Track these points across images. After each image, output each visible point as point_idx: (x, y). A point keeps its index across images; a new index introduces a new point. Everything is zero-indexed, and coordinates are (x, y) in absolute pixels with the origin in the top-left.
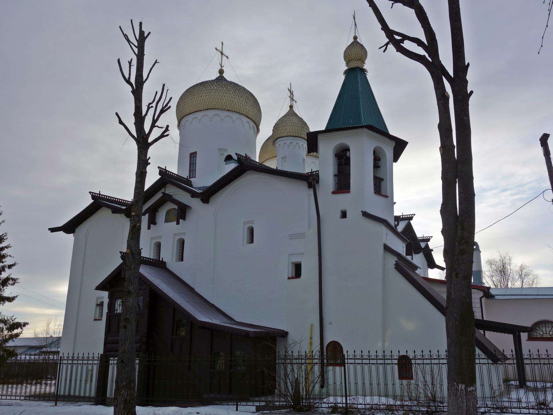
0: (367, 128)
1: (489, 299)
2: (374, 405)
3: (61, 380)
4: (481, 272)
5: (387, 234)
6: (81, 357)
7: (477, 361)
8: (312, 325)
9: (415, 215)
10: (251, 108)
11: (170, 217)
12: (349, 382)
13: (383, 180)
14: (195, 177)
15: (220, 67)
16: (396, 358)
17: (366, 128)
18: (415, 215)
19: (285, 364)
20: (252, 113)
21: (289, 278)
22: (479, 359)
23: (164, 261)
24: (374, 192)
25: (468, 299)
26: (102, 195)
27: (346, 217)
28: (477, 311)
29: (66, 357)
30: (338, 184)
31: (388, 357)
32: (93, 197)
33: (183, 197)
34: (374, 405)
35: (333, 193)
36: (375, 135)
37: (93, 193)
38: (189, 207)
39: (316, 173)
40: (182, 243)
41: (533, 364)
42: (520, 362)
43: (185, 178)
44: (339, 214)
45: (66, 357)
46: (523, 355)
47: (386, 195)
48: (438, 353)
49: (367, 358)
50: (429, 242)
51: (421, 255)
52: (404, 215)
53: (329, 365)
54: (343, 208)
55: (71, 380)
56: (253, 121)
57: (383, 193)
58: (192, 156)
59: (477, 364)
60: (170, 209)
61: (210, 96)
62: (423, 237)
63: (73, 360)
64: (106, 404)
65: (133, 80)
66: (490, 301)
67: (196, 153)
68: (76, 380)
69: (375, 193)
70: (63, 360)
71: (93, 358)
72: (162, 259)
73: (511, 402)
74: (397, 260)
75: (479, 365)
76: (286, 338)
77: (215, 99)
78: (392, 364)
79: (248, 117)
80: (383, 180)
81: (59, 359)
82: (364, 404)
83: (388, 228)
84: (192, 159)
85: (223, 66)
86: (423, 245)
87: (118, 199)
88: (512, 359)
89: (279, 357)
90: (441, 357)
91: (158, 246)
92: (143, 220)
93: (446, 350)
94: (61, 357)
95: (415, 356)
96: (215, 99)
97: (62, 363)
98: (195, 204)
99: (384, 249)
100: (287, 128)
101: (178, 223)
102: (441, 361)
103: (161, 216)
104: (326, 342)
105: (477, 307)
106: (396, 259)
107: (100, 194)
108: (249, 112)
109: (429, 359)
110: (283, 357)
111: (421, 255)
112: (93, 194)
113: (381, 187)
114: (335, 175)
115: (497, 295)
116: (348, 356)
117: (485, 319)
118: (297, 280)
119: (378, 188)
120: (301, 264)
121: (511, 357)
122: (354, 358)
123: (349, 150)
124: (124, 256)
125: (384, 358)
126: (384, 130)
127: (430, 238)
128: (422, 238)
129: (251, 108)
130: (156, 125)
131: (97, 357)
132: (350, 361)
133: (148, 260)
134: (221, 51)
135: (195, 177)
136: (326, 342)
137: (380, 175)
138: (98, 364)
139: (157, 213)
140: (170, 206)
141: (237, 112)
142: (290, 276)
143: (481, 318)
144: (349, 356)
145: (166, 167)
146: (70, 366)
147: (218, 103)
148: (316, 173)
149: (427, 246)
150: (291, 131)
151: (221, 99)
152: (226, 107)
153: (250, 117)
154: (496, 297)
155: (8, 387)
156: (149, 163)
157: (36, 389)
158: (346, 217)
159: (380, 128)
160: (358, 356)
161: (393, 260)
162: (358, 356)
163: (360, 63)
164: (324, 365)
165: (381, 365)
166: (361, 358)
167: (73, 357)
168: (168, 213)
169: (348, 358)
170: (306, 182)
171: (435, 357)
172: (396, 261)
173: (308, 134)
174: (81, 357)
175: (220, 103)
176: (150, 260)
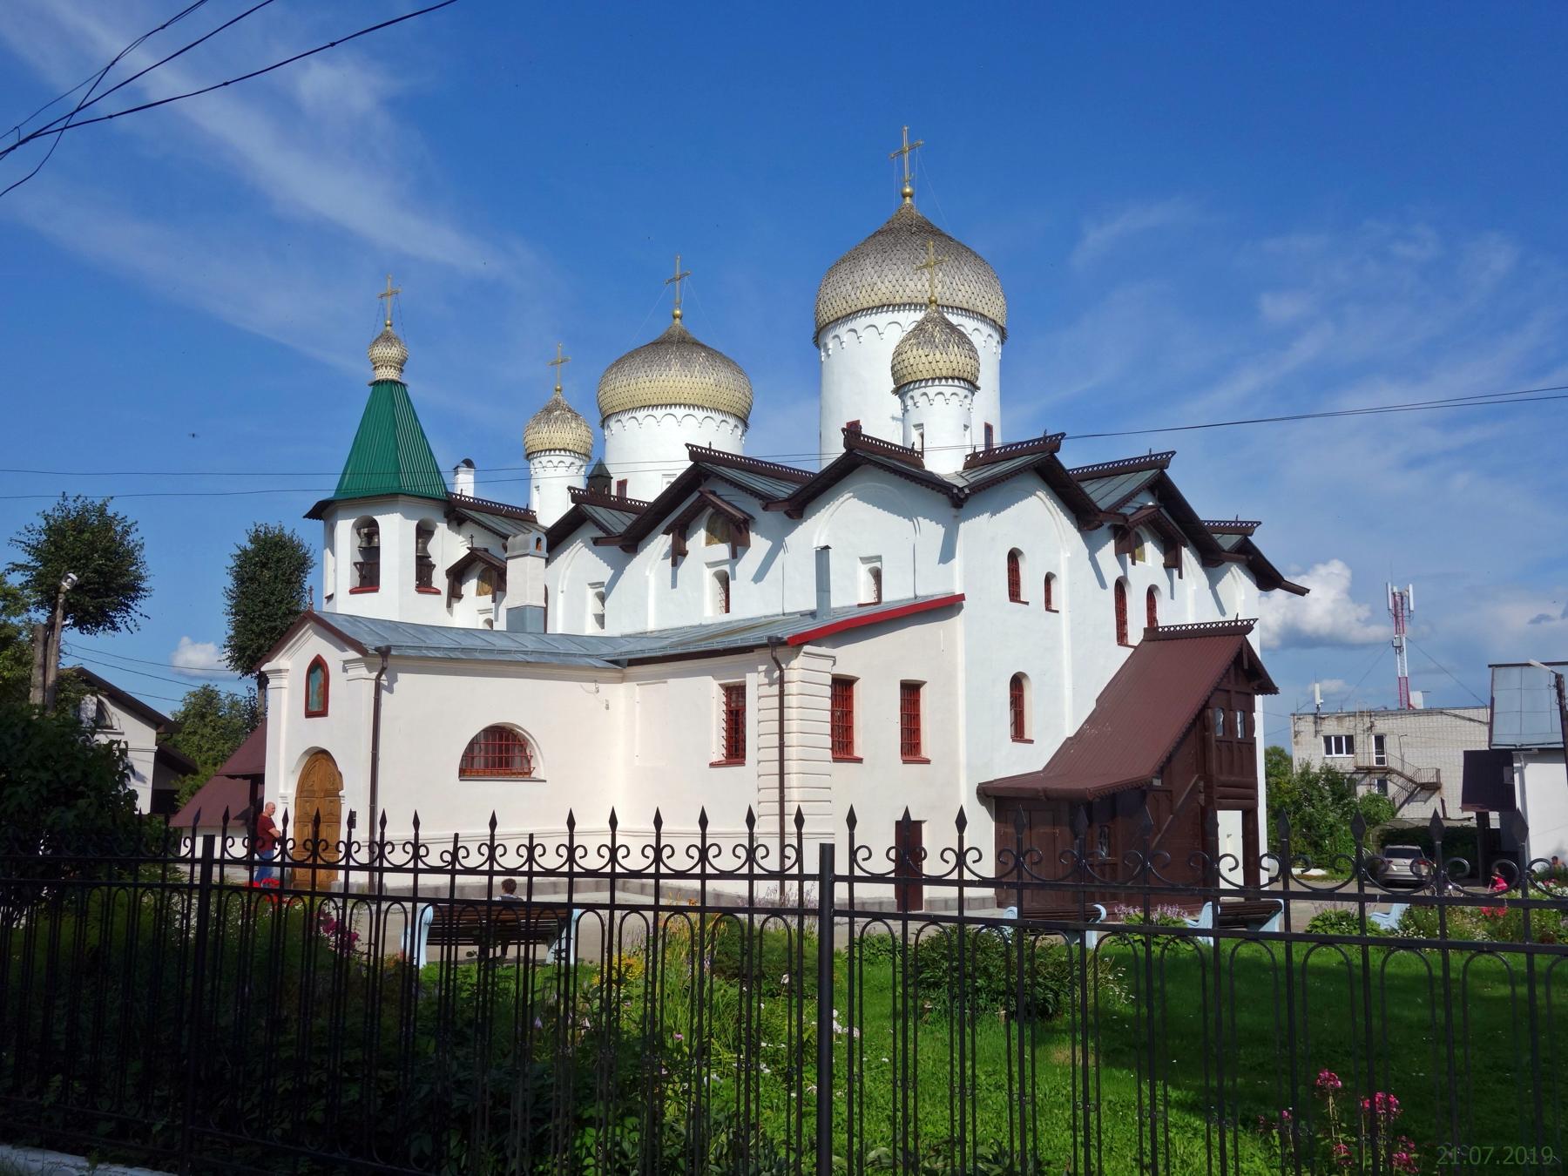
6: (680, 848)
9: (1174, 453)
18: (1174, 453)
21: (712, 765)
26: (715, 451)
29: (727, 849)
37: (693, 446)
39: (1145, 460)
42: (422, 1095)
45: (727, 849)
46: (893, 854)
50: (1167, 468)
52: (1154, 455)
70: (851, 879)
76: (1268, 747)
81: (812, 865)
87: (699, 447)
94: (827, 852)
107: (710, 449)
110: (363, 857)
116: (853, 853)
122: (955, 876)
124: (576, 496)
148: (1145, 460)
166: (310, 861)
169: (858, 872)
174: (680, 848)
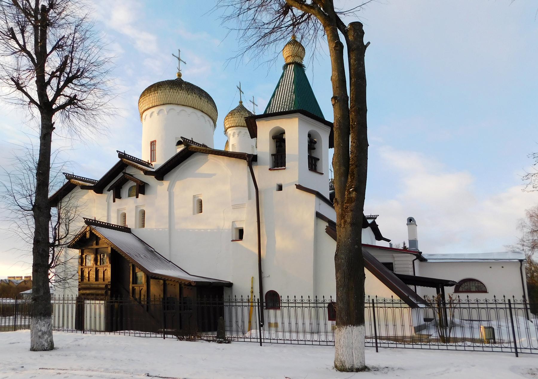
0: (301, 113)
1: (422, 262)
4: (416, 242)
5: (320, 204)
8: (253, 277)
10: (205, 104)
11: (132, 192)
13: (318, 159)
14: (156, 161)
15: (178, 70)
17: (299, 112)
20: (207, 108)
22: (377, 303)
23: (128, 227)
24: (309, 169)
25: (356, 246)
27: (282, 190)
28: (410, 270)
30: (274, 162)
31: (239, 301)
32: (67, 177)
33: (141, 176)
35: (270, 169)
36: (314, 122)
38: (147, 184)
40: (143, 213)
41: (453, 308)
43: (146, 162)
44: (275, 187)
45: (75, 298)
47: (321, 172)
51: (369, 229)
53: (268, 308)
55: (63, 316)
56: (208, 115)
57: (318, 171)
58: (153, 144)
60: (133, 186)
61: (165, 93)
62: (371, 216)
63: (64, 300)
65: (30, 47)
66: (423, 263)
67: (155, 141)
69: (309, 170)
71: (72, 299)
72: (127, 226)
73: (488, 320)
74: (328, 225)
77: (170, 96)
79: (203, 112)
80: (318, 159)
83: (321, 199)
84: (152, 146)
85: (180, 70)
86: (370, 221)
91: (124, 216)
95: (324, 301)
96: (170, 96)
98: (151, 180)
99: (316, 216)
100: (236, 119)
101: (137, 197)
103: (125, 191)
104: (266, 290)
105: (410, 267)
106: (327, 224)
108: (204, 107)
111: (369, 229)
112: (66, 175)
113: (316, 166)
114: (272, 155)
115: (429, 259)
117: (416, 275)
118: (240, 242)
119: (314, 167)
120: (243, 229)
123: (284, 133)
125: (316, 302)
126: (319, 116)
127: (377, 216)
128: (370, 216)
129: (205, 104)
130: (61, 93)
132: (379, 305)
133: (120, 227)
134: (178, 57)
135: (156, 161)
136: (266, 290)
137: (314, 155)
138: (281, 303)
139: (121, 190)
140: (132, 184)
141: (189, 106)
142: (234, 239)
143: (411, 274)
145: (124, 151)
146: (61, 306)
147: (173, 99)
149: (374, 222)
150: (239, 122)
151: (175, 96)
152: (181, 102)
154: (429, 261)
155: (9, 319)
156: (54, 128)
157: (21, 322)
158: (282, 190)
159: (316, 114)
161: (324, 225)
163: (297, 58)
164: (263, 308)
168: (130, 189)
171: (240, 301)
172: (327, 226)
173: (245, 119)
175: (175, 99)
176: (105, 224)
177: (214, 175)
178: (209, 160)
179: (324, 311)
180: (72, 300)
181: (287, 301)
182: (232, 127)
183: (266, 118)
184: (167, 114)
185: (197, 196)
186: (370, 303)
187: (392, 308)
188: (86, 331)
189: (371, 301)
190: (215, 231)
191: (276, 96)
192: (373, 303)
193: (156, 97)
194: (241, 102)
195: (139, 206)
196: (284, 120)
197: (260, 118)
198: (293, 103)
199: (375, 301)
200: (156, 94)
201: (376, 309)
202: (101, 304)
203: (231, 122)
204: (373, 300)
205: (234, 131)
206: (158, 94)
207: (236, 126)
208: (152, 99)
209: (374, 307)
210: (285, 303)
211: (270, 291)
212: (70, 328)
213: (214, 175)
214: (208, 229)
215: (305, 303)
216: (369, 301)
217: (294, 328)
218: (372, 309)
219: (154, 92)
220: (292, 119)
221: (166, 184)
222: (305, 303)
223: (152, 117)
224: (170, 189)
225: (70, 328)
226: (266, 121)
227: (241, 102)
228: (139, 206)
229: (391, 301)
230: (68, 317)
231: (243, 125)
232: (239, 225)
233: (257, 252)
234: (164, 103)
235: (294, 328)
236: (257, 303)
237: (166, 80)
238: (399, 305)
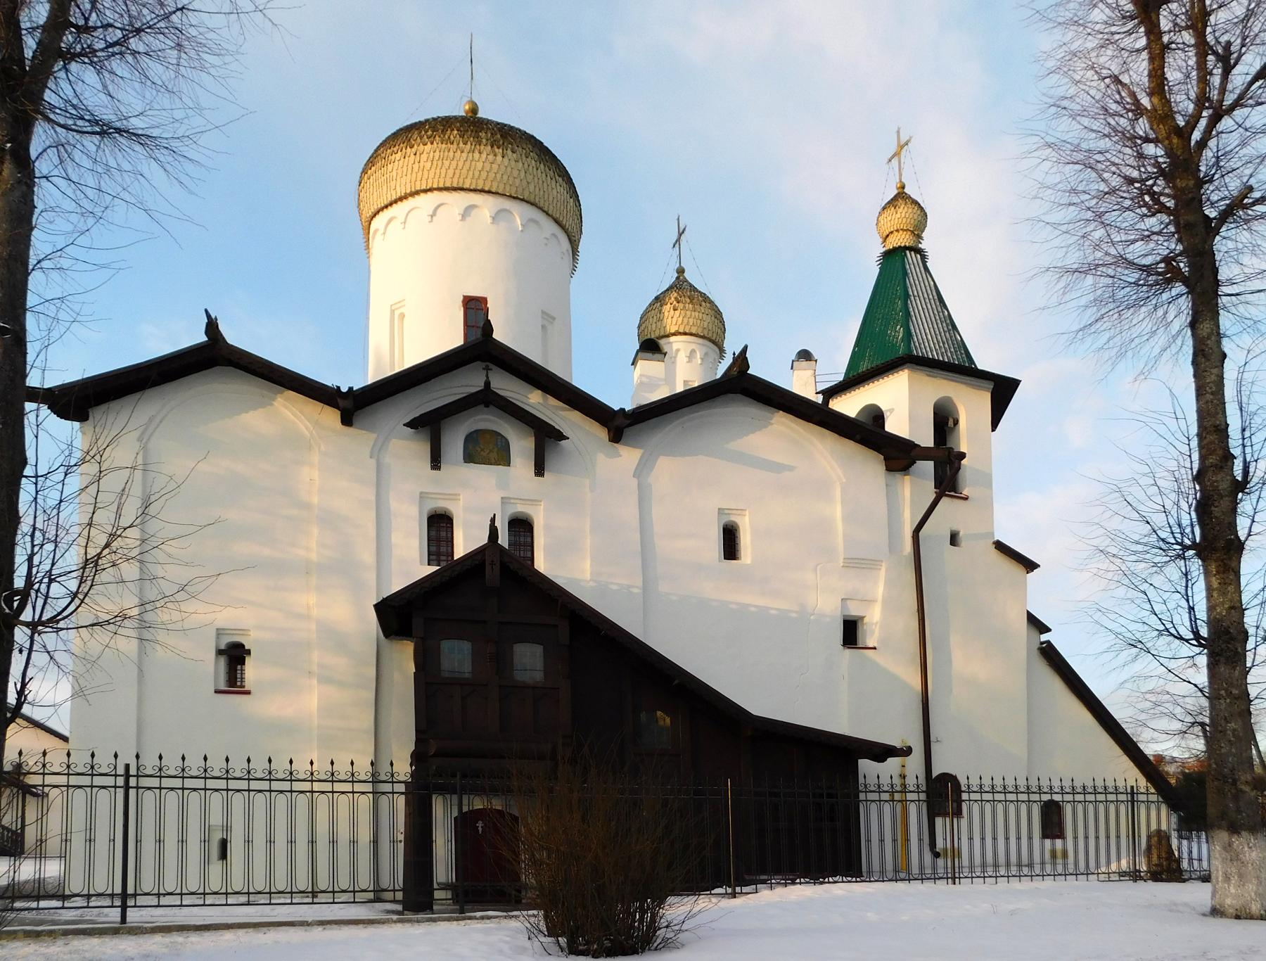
2: (297, 893)
3: (138, 841)
7: (862, 796)
12: (139, 838)
16: (402, 778)
19: (904, 803)
22: (866, 792)
34: (297, 893)
48: (289, 765)
49: (874, 789)
54: (955, 528)
59: (964, 801)
64: (521, 901)
68: (1086, 838)
70: (1137, 794)
75: (967, 802)
78: (270, 791)
82: (269, 891)
88: (369, 782)
89: (866, 786)
90: (210, 773)
92: (462, 393)
93: (372, 761)
97: (1135, 799)
102: (358, 787)
104: (936, 772)
109: (328, 781)
110: (899, 788)
116: (138, 769)
121: (63, 769)
131: (915, 786)
136: (936, 772)
144: (141, 768)
153: (541, 205)
160: (886, 786)
162: (886, 786)
165: (172, 794)
167: (904, 785)
170: (883, 457)
171: (874, 789)
177: (791, 468)
178: (772, 424)
179: (247, 802)
180: (1117, 794)
181: (63, 769)
182: (691, 334)
183: (931, 370)
184: (522, 231)
185: (726, 512)
186: (116, 776)
187: (268, 794)
188: (45, 857)
189: (121, 771)
190: (794, 615)
191: (914, 318)
192: (127, 776)
193: (495, 166)
194: (681, 271)
195: (512, 501)
196: (945, 382)
197: (917, 364)
198: (963, 352)
199: (133, 771)
200: (499, 158)
201: (132, 792)
202: (1087, 803)
203: (691, 320)
204: (127, 767)
205: (693, 346)
206: (506, 160)
207: (703, 337)
208: (480, 165)
209: (127, 787)
210: (196, 777)
211: (944, 773)
212: (1071, 868)
213: (791, 468)
214: (772, 609)
215: (192, 777)
216: (115, 768)
217: (1025, 860)
218: (120, 792)
219: (492, 147)
220: (977, 391)
221: (628, 456)
222: (192, 777)
223: (468, 219)
224: (642, 470)
225: (1071, 868)
226: (930, 376)
227: (681, 271)
228: (512, 501)
229: (87, 770)
230: (1118, 837)
231: (687, 331)
232: (854, 611)
233: (917, 683)
234: (465, 187)
235: (1025, 860)
236: (122, 778)
237: (512, 125)
238: (50, 780)
